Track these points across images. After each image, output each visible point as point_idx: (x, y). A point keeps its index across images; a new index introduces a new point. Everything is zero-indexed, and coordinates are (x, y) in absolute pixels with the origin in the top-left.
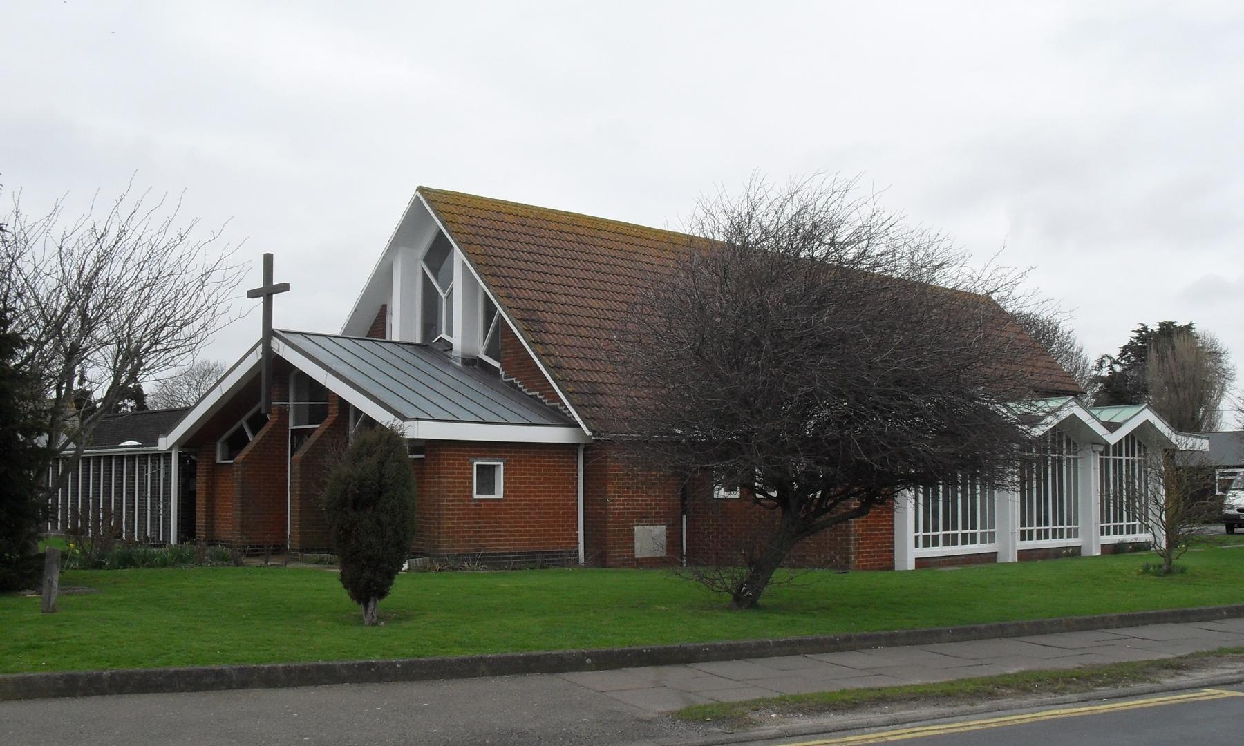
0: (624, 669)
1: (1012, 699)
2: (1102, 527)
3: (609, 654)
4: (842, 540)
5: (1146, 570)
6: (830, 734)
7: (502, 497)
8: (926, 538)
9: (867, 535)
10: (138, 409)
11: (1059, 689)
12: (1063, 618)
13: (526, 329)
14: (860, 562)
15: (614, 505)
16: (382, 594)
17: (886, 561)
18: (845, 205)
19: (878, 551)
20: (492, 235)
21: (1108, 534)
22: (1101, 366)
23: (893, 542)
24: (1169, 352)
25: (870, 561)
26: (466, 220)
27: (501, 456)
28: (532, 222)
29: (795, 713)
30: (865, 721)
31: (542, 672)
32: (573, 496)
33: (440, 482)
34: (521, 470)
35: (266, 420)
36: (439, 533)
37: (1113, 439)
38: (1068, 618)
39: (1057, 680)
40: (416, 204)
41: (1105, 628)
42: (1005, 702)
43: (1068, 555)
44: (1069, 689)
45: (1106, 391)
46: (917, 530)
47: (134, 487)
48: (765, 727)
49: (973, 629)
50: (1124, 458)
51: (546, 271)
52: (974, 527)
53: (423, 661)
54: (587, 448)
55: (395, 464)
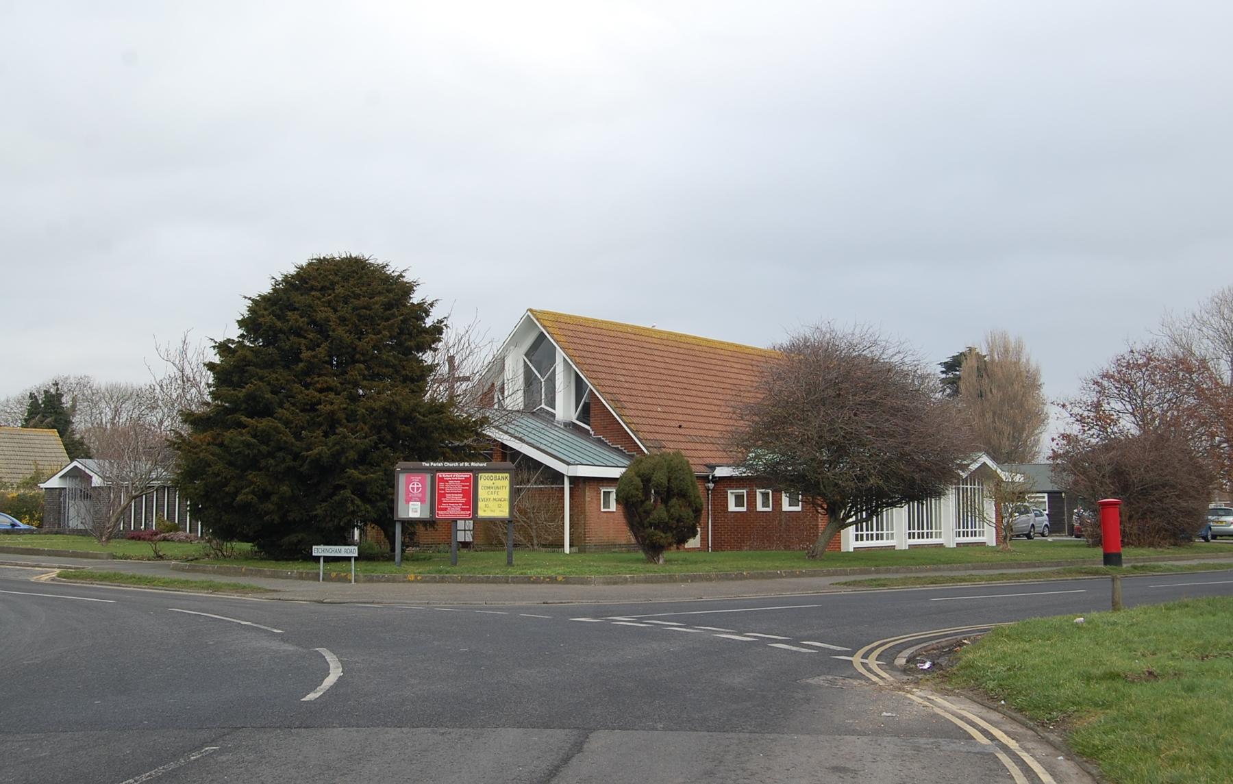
2: (909, 533)
50: (969, 486)
52: (882, 530)
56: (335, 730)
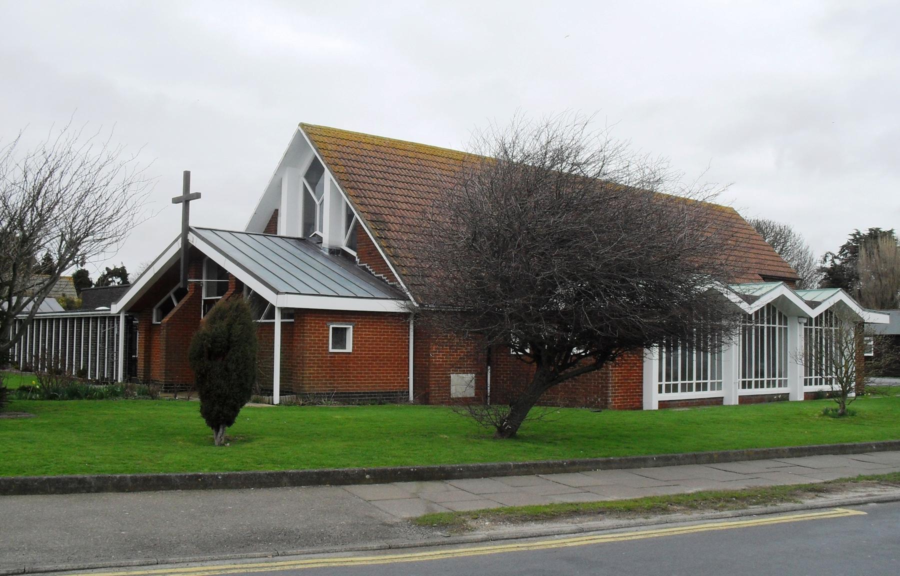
0: (396, 483)
1: (680, 514)
3: (384, 472)
4: (602, 386)
5: (826, 413)
6: (525, 539)
7: (351, 351)
8: (668, 386)
9: (621, 383)
10: (123, 283)
11: (718, 507)
12: (745, 450)
13: (374, 227)
14: (615, 403)
15: (435, 358)
16: (230, 422)
17: (638, 405)
18: (584, 135)
19: (630, 396)
20: (353, 159)
21: (811, 384)
22: (825, 260)
23: (642, 389)
24: (875, 251)
25: (624, 402)
26: (334, 147)
27: (351, 321)
28: (385, 150)
29: (504, 522)
30: (556, 529)
31: (331, 484)
32: (405, 351)
33: (304, 340)
34: (366, 331)
35: (187, 292)
36: (303, 377)
37: (814, 313)
38: (749, 449)
39: (719, 499)
40: (298, 135)
41: (778, 458)
42: (673, 517)
43: (778, 400)
44: (727, 507)
45: (828, 279)
46: (660, 380)
47: (97, 340)
48: (478, 532)
49: (673, 457)
50: (777, 326)
51: (392, 185)
52: (705, 378)
53: (239, 474)
54: (416, 316)
55: (240, 326)
56: (716, 452)
